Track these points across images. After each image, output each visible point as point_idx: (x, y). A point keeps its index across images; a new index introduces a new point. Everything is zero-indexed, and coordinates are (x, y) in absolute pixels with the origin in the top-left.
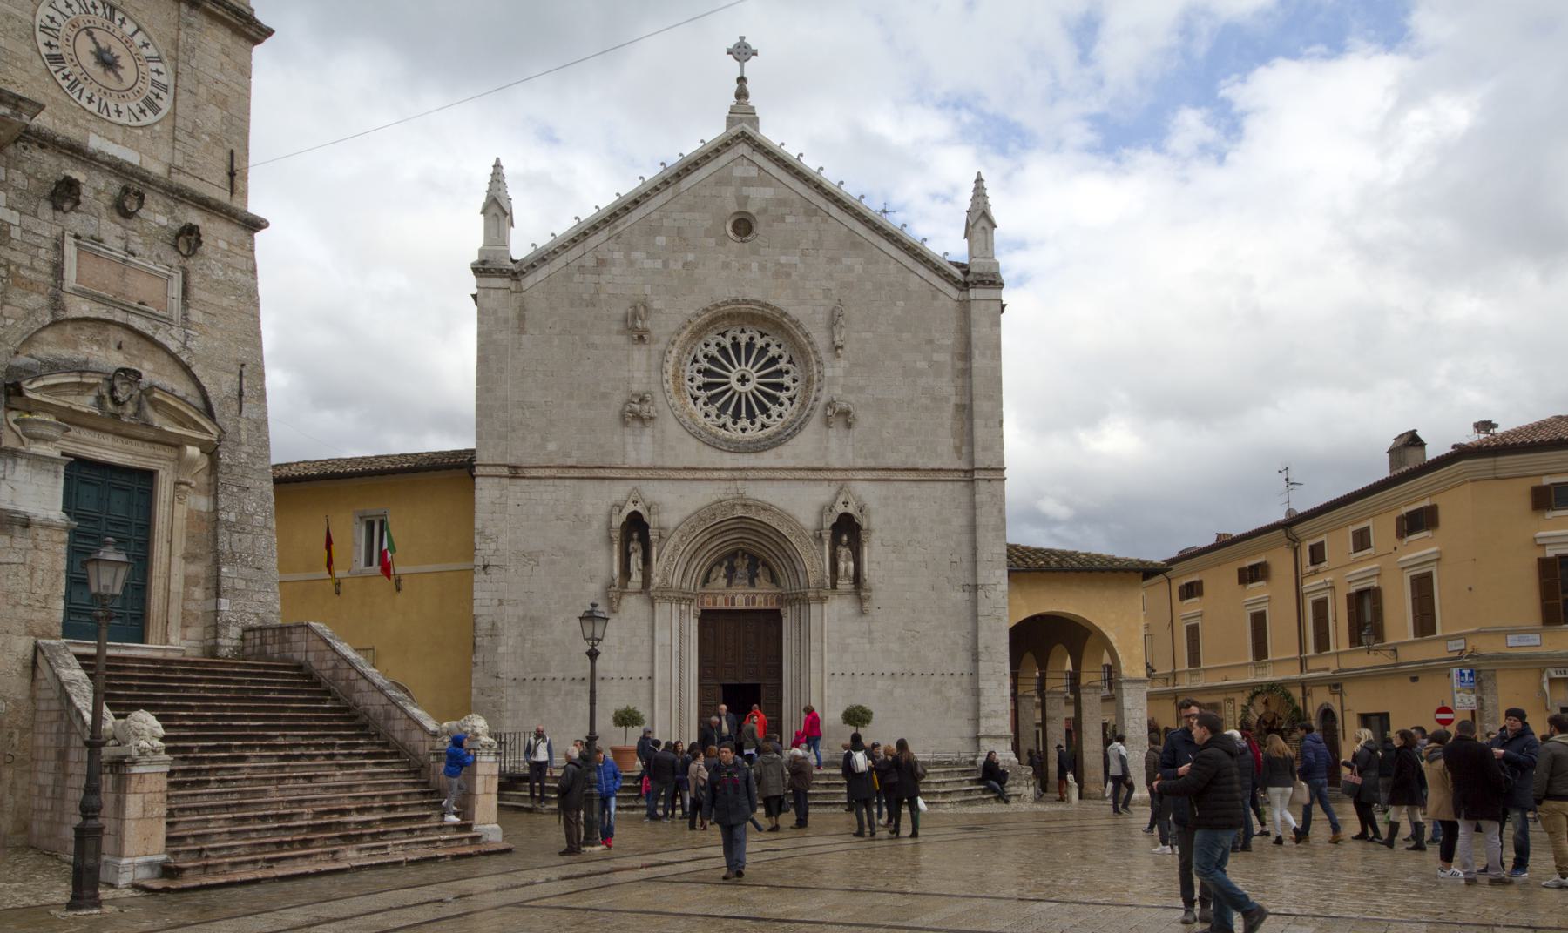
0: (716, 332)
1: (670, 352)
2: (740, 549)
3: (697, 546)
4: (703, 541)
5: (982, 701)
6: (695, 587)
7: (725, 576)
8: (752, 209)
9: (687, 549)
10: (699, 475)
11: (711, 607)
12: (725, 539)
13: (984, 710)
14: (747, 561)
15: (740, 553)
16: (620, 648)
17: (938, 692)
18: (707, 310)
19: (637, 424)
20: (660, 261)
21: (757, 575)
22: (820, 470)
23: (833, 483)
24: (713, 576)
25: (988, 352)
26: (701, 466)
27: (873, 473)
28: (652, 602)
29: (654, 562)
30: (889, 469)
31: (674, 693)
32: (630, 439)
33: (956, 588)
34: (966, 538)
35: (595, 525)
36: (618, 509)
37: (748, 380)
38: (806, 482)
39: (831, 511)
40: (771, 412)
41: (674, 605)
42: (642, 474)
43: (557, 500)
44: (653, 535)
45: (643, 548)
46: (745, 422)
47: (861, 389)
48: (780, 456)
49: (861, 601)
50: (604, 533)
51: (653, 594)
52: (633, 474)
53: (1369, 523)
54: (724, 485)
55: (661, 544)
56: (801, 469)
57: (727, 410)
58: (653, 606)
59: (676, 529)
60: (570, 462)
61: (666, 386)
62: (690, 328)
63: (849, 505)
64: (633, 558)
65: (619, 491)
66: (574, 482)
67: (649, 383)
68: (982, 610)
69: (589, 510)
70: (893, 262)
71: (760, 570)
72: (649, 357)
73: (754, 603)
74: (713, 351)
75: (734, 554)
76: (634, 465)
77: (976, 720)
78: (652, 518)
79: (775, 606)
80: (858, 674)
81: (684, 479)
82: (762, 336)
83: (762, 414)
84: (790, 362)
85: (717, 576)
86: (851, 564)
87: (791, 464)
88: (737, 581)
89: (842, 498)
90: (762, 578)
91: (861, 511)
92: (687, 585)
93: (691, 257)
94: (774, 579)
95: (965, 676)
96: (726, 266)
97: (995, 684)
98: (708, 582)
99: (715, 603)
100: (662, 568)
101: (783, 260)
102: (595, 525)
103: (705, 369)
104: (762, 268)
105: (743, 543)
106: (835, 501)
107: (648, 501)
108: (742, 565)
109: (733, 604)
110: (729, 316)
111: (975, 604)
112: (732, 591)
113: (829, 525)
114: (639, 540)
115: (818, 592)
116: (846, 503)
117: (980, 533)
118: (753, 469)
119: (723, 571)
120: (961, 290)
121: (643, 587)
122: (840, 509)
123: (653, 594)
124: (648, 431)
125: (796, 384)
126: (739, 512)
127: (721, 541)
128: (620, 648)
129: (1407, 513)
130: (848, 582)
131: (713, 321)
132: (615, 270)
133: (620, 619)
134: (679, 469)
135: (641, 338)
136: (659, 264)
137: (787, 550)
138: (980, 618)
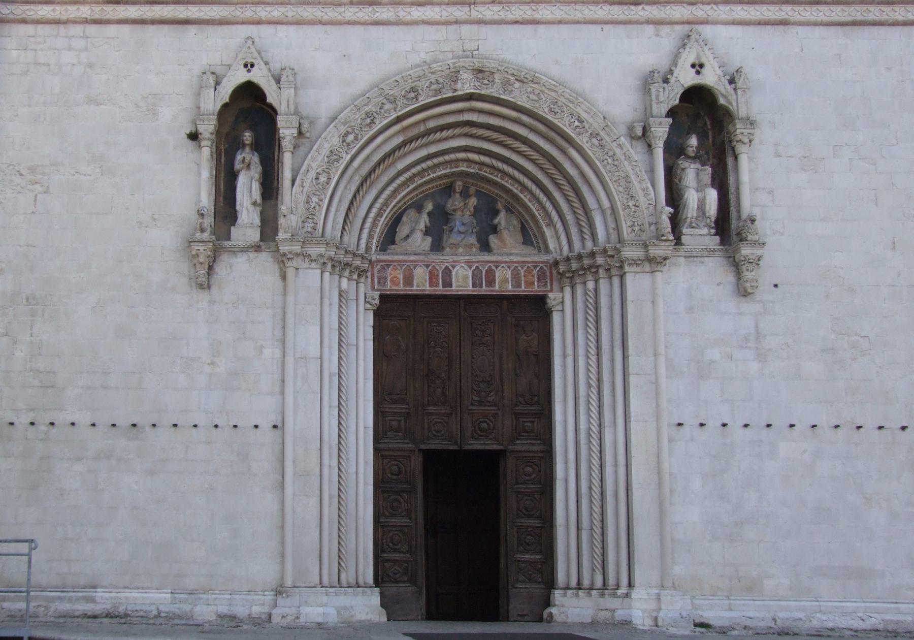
2: (462, 174)
3: (376, 158)
4: (388, 147)
6: (368, 249)
7: (427, 233)
9: (356, 163)
11: (401, 288)
14: (473, 201)
15: (459, 185)
16: (212, 363)
21: (495, 230)
23: (666, 29)
24: (403, 230)
28: (282, 260)
31: (326, 461)
36: (212, 81)
39: (666, 81)
41: (327, 275)
43: (91, 66)
44: (286, 131)
45: (262, 162)
49: (736, 265)
51: (283, 249)
54: (440, 33)
55: (302, 150)
63: (704, 71)
64: (242, 181)
71: (502, 219)
73: (491, 282)
79: (536, 289)
85: (412, 231)
86: (712, 195)
88: (455, 238)
89: (689, 57)
90: (505, 233)
91: (732, 81)
92: (354, 240)
98: (393, 242)
99: (409, 280)
100: (303, 198)
106: (675, 63)
107: (276, 66)
109: (447, 283)
112: (441, 260)
113: (664, 109)
114: (256, 147)
116: (698, 67)
121: (264, 237)
122: (686, 78)
123: (283, 249)
126: (467, 85)
127: (423, 153)
128: (212, 363)
130: (705, 231)
133: (212, 302)
137: (568, 166)
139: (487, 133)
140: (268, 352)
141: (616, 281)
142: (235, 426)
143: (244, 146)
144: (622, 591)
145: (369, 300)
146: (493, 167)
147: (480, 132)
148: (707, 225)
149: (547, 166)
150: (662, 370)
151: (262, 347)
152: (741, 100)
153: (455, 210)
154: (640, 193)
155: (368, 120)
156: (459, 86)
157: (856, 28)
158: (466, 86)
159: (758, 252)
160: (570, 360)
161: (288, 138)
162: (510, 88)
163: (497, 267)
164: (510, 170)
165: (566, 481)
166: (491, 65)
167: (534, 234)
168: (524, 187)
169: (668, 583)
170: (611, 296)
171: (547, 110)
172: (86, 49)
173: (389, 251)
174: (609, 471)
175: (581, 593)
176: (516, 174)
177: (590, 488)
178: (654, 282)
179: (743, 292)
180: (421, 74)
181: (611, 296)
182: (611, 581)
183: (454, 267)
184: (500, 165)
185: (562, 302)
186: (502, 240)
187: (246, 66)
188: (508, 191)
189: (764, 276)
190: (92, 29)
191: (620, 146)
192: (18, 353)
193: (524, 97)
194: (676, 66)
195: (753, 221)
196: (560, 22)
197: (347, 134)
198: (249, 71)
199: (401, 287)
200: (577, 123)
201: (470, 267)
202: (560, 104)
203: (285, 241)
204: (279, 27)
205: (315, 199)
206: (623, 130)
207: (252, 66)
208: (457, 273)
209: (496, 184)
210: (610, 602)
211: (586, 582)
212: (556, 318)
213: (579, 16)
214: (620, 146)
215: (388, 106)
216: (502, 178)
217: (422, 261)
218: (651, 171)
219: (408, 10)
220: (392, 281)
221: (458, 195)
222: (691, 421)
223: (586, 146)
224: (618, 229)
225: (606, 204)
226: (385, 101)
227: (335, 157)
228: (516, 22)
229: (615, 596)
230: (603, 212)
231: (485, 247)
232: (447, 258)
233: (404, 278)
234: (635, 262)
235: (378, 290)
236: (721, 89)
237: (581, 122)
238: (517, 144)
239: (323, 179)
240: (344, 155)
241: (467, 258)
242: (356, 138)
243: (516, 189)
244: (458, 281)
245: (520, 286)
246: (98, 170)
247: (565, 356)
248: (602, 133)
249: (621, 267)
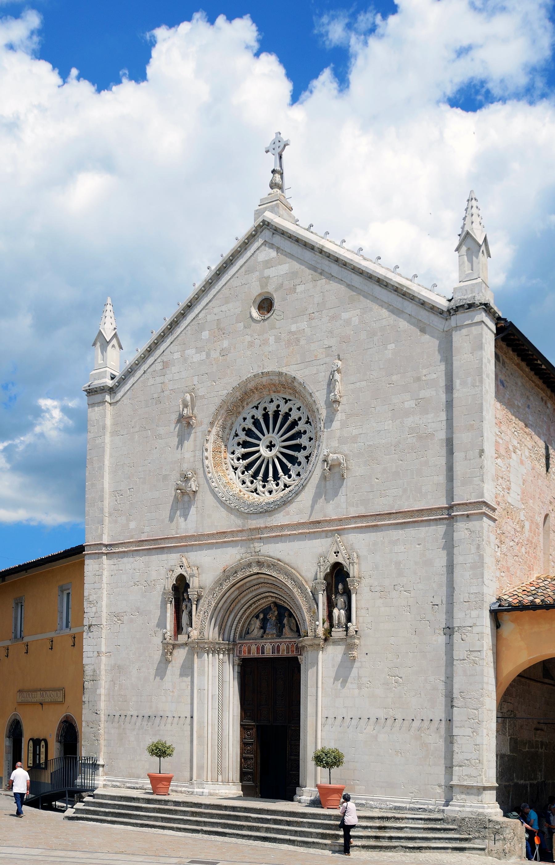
4: (233, 596)
5: (456, 748)
8: (270, 289)
9: (220, 605)
11: (246, 655)
13: (457, 758)
20: (204, 353)
25: (469, 380)
33: (437, 631)
40: (291, 472)
41: (211, 655)
46: (272, 485)
47: (354, 439)
48: (288, 514)
57: (292, 456)
61: (206, 462)
63: (339, 555)
65: (173, 558)
68: (457, 654)
73: (278, 651)
77: (449, 768)
93: (225, 344)
96: (251, 344)
97: (468, 731)
101: (294, 328)
103: (244, 442)
104: (278, 340)
109: (263, 653)
111: (450, 646)
116: (337, 553)
117: (458, 572)
132: (174, 369)
136: (203, 356)
163: (281, 644)
183: (265, 645)
192: (116, 688)
201: (271, 644)
208: (266, 648)
233: (248, 650)
244: (267, 651)
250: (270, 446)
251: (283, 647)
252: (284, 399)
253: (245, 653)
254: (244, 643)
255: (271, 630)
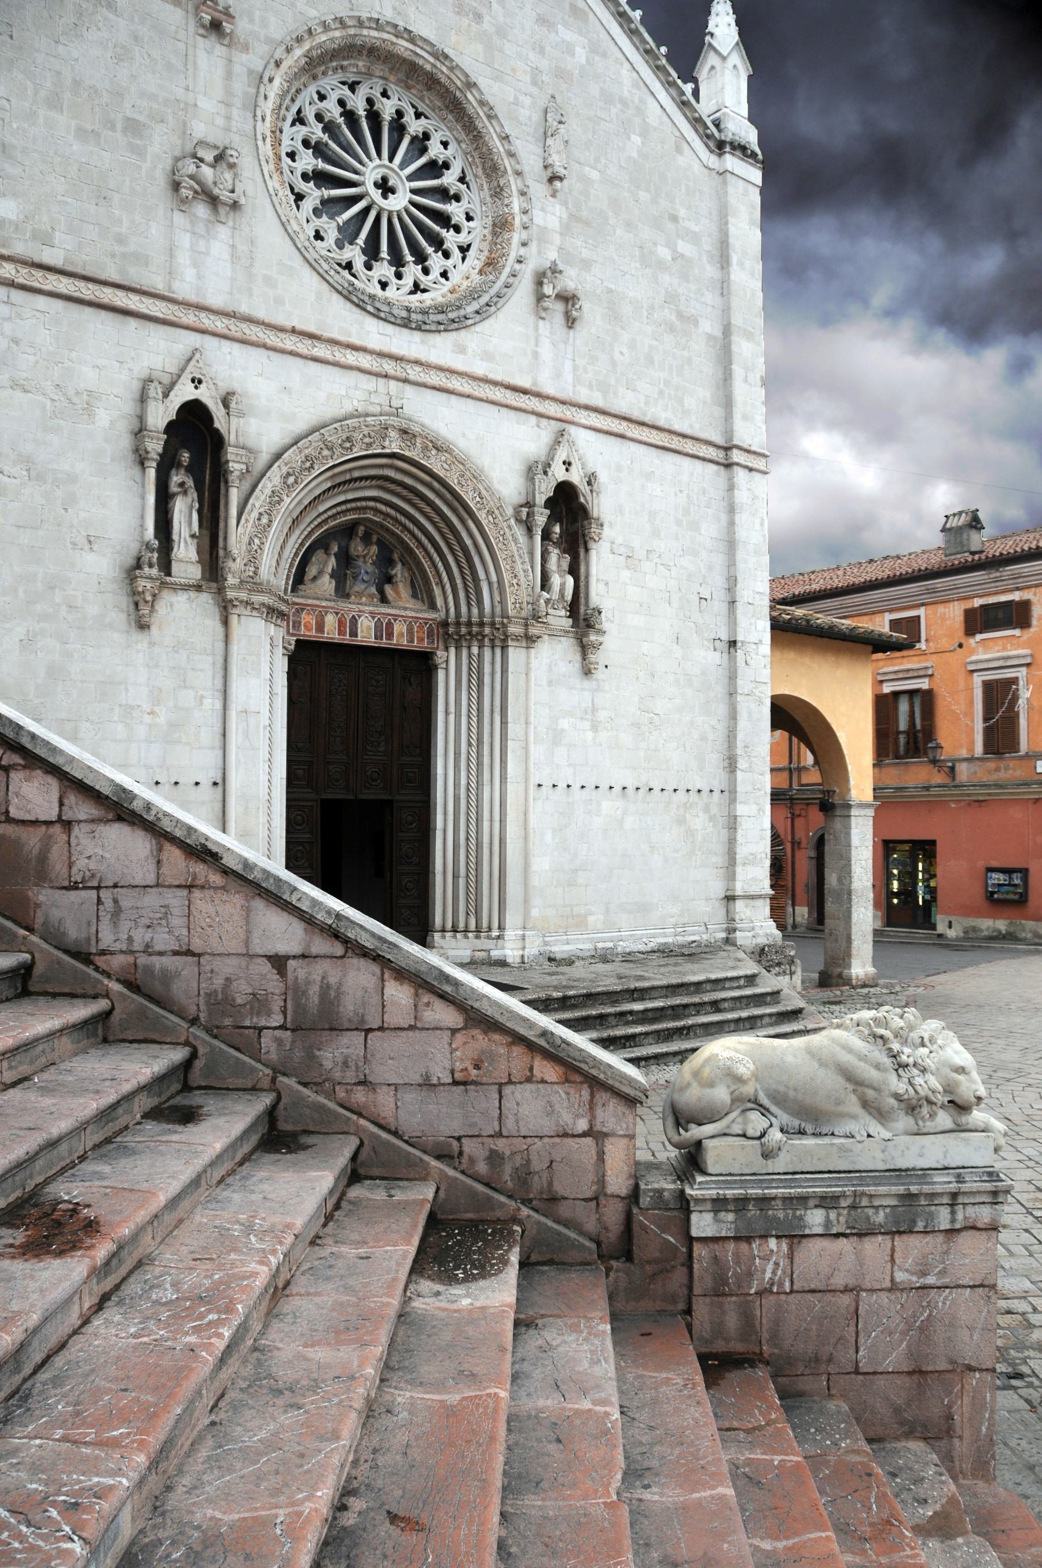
0: (340, 76)
1: (271, 80)
10: (321, 351)
11: (312, 634)
12: (350, 496)
15: (361, 530)
17: (681, 821)
18: (342, 22)
19: (201, 210)
21: (389, 579)
22: (525, 392)
24: (312, 571)
26: (326, 334)
27: (601, 417)
28: (225, 609)
29: (233, 521)
30: (625, 419)
32: (185, 240)
34: (719, 560)
35: (103, 417)
37: (393, 191)
38: (503, 410)
39: (545, 473)
42: (207, 321)
48: (462, 350)
49: (584, 649)
50: (126, 442)
51: (231, 594)
52: (189, 318)
53: (921, 612)
56: (495, 383)
58: (225, 622)
59: (278, 456)
60: (48, 257)
62: (307, 46)
66: (58, 304)
67: (228, 130)
69: (87, 377)
70: (627, 65)
72: (229, 75)
73: (390, 636)
74: (333, 111)
75: (348, 530)
76: (193, 298)
78: (234, 421)
79: (425, 645)
80: (705, 793)
81: (292, 353)
82: (418, 115)
83: (416, 263)
84: (462, 180)
85: (321, 572)
87: (480, 369)
90: (401, 585)
91: (589, 483)
94: (422, 591)
95: (716, 794)
99: (320, 627)
100: (246, 539)
102: (103, 417)
105: (376, 511)
107: (224, 387)
108: (365, 554)
109: (354, 633)
110: (373, 52)
112: (349, 607)
115: (526, 625)
116: (567, 464)
117: (740, 555)
118: (417, 362)
119: (332, 562)
120: (712, 152)
122: (559, 473)
123: (231, 594)
124: (223, 232)
125: (471, 224)
127: (342, 498)
128: (152, 713)
129: (982, 606)
131: (349, 50)
133: (152, 644)
134: (282, 330)
135: (216, 26)
138: (739, 698)
139: (399, 489)
140: (208, 702)
141: (498, 651)
142: (176, 783)
143: (179, 465)
144: (495, 933)
145: (286, 645)
146: (396, 520)
147: (393, 487)
148: (564, 608)
149: (446, 530)
150: (531, 738)
151: (202, 697)
152: (595, 502)
153: (358, 556)
154: (522, 572)
155: (308, 464)
156: (387, 443)
157: (664, 452)
158: (393, 445)
159: (601, 639)
160: (452, 717)
161: (236, 473)
162: (428, 454)
163: (395, 620)
164: (411, 526)
165: (445, 831)
166: (416, 429)
167: (419, 586)
168: (420, 544)
169: (529, 925)
170: (493, 663)
171: (456, 481)
172: (9, 319)
173: (301, 593)
174: (486, 825)
175: (458, 935)
176: (416, 531)
177: (467, 839)
178: (528, 657)
179: (587, 672)
180: (357, 425)
181: (493, 663)
182: (485, 924)
183: (360, 617)
184: (403, 519)
185: (447, 661)
186: (397, 593)
187: (193, 381)
188: (402, 542)
189: (599, 657)
190: (17, 296)
191: (510, 527)
193: (439, 465)
194: (552, 459)
195: (600, 613)
196: (468, 396)
197: (289, 474)
198: (196, 388)
199: (314, 633)
200: (478, 499)
201: (373, 618)
202: (466, 477)
203: (234, 587)
204: (224, 342)
205: (257, 541)
206: (510, 511)
207: (200, 382)
209: (393, 533)
210: (484, 943)
211: (461, 926)
212: (441, 674)
213: (482, 395)
214: (510, 527)
215: (326, 452)
216: (402, 532)
217: (332, 608)
218: (531, 554)
219: (343, 351)
220: (305, 626)
221: (358, 540)
222: (547, 783)
223: (484, 522)
224: (503, 602)
225: (494, 578)
226: (323, 446)
227: (277, 498)
228: (434, 388)
229: (489, 938)
230: (490, 584)
231: (384, 600)
232: (354, 606)
234: (517, 638)
235: (293, 635)
236: (582, 488)
237: (482, 498)
238: (422, 505)
239: (265, 520)
240: (285, 498)
241: (371, 608)
242: (296, 482)
243: (412, 544)
245: (413, 642)
246: (25, 473)
247: (447, 713)
248: (497, 512)
249: (505, 640)
250: (385, 187)
251: (399, 628)
252: (424, 291)
253: (308, 627)
254: (308, 605)
255: (364, 587)
